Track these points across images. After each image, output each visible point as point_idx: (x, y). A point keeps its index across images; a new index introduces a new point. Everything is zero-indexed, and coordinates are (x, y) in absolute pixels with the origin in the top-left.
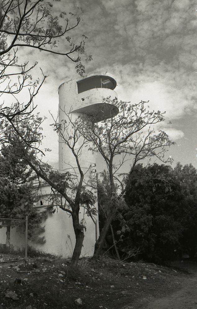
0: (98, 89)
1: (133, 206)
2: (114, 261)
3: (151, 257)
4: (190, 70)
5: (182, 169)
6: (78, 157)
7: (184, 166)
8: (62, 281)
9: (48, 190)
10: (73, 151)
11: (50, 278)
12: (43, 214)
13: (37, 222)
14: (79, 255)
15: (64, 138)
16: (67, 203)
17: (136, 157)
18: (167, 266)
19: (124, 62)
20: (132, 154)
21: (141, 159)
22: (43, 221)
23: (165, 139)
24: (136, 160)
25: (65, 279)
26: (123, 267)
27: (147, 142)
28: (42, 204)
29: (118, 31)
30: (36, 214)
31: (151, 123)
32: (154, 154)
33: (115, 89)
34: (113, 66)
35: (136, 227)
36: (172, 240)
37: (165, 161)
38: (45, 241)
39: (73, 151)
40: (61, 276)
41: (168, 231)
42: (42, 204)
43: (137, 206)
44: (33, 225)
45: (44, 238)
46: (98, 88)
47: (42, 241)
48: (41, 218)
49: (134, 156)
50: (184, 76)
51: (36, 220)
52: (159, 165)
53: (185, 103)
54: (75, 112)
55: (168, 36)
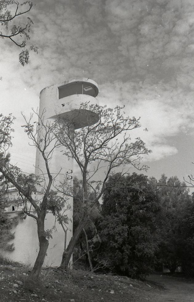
0: (79, 95)
1: (108, 215)
2: (87, 273)
3: (125, 270)
4: (187, 90)
5: (167, 181)
6: (48, 161)
7: (169, 178)
8: (15, 292)
9: (16, 196)
10: (43, 154)
11: (3, 288)
12: (14, 220)
13: (7, 228)
14: (42, 264)
15: (35, 141)
16: (33, 207)
17: (111, 165)
18: (141, 280)
19: (124, 80)
20: (108, 161)
21: (116, 166)
22: (13, 227)
23: (141, 147)
24: (110, 167)
25: (21, 290)
26: (90, 279)
27: (123, 148)
28: (13, 209)
29: (121, 51)
30: (7, 220)
31: (127, 130)
32: (129, 162)
33: (96, 97)
34: (113, 83)
35: (111, 237)
36: (147, 253)
37: (139, 169)
38: (14, 248)
39: (43, 154)
40: (16, 286)
41: (144, 243)
42: (13, 209)
43: (112, 216)
44: (3, 231)
45: (12, 245)
46: (79, 94)
47: (11, 248)
48: (11, 224)
49: (108, 163)
50: (181, 95)
51: (6, 225)
52: (137, 175)
53: (180, 121)
54: (52, 117)
55: (167, 57)
